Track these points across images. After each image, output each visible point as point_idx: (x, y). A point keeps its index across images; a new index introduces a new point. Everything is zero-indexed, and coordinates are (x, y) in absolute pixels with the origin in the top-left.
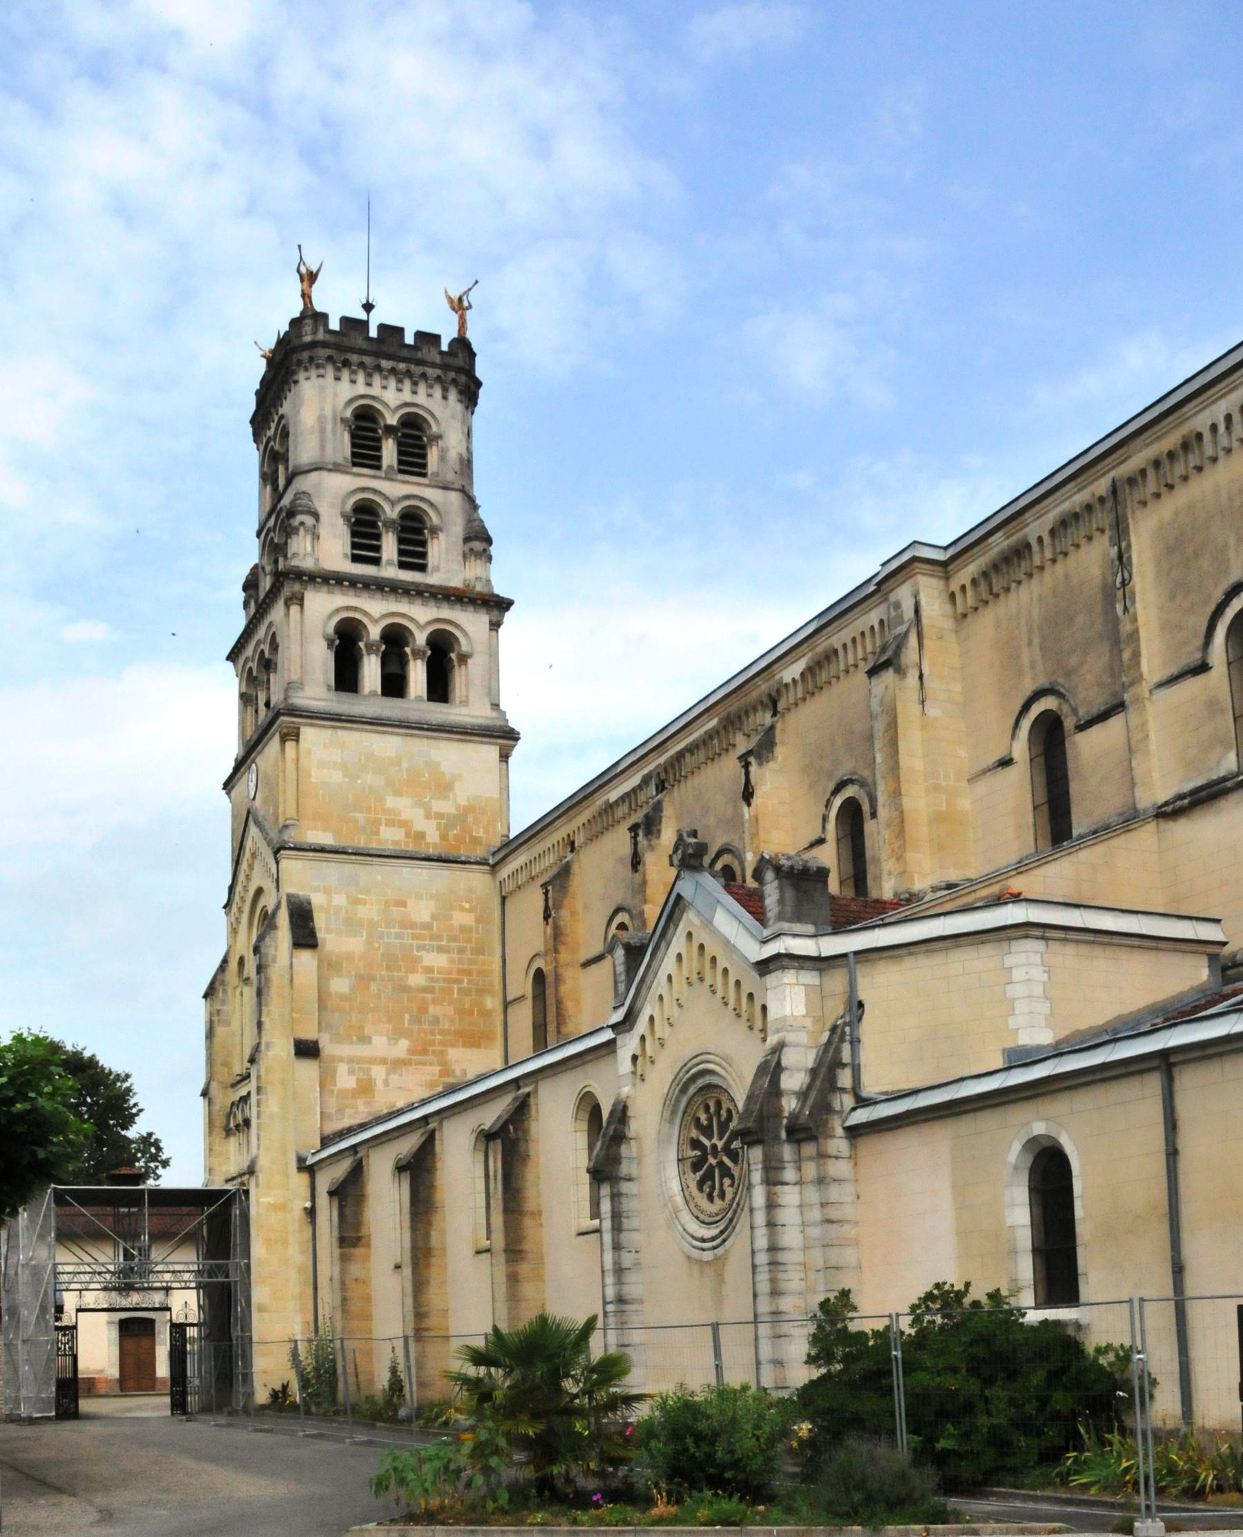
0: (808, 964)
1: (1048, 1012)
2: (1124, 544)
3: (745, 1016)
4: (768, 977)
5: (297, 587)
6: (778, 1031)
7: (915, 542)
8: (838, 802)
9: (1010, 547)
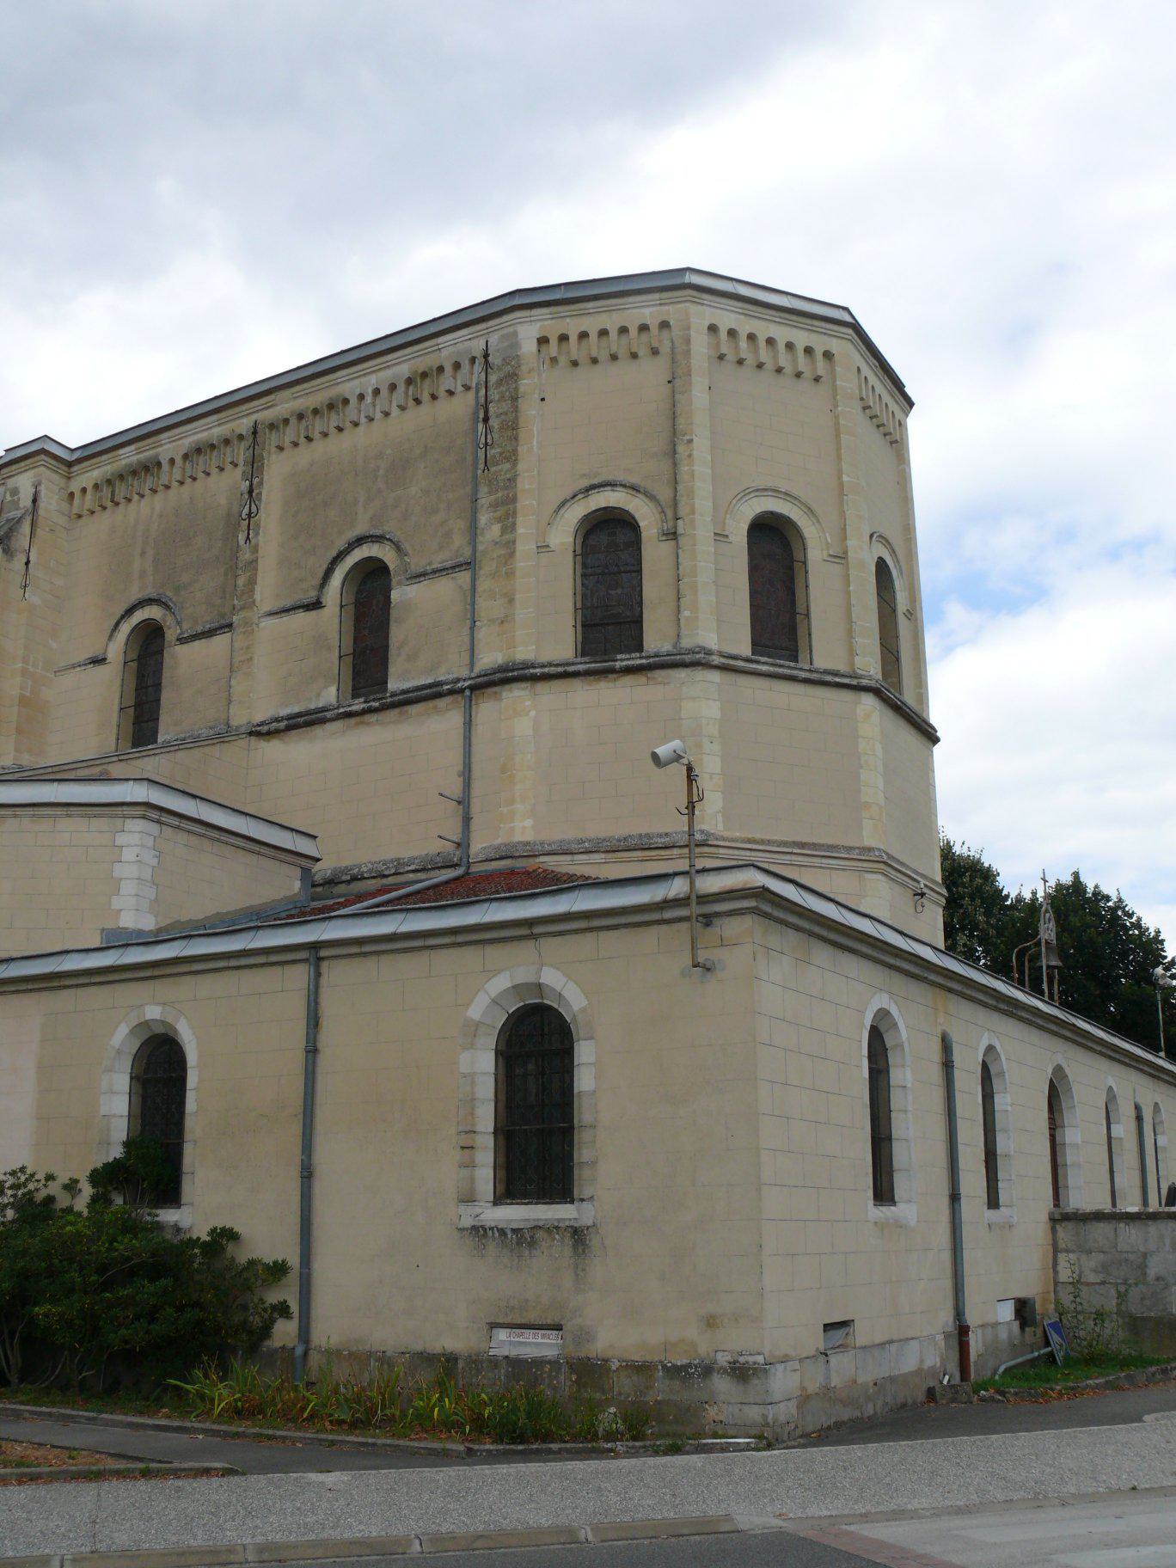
1: (153, 897)
2: (256, 481)
7: (46, 436)
9: (139, 462)
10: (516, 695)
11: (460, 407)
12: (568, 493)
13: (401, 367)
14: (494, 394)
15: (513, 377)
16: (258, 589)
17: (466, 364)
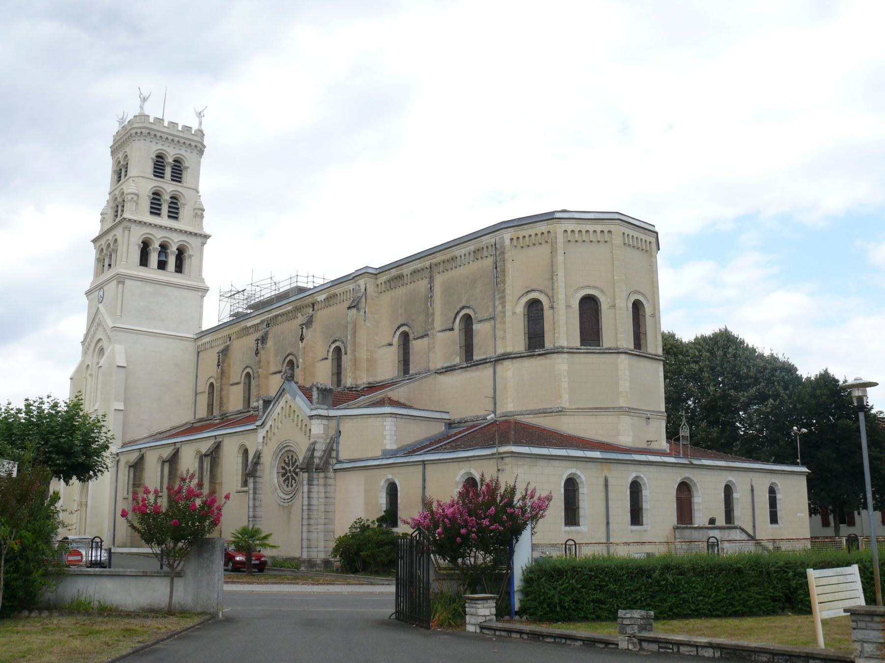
0: (325, 418)
3: (303, 431)
4: (312, 421)
5: (129, 224)
6: (314, 438)
8: (333, 346)
10: (507, 364)
11: (488, 262)
12: (521, 294)
13: (471, 247)
14: (498, 259)
15: (503, 253)
16: (435, 322)
17: (490, 247)
